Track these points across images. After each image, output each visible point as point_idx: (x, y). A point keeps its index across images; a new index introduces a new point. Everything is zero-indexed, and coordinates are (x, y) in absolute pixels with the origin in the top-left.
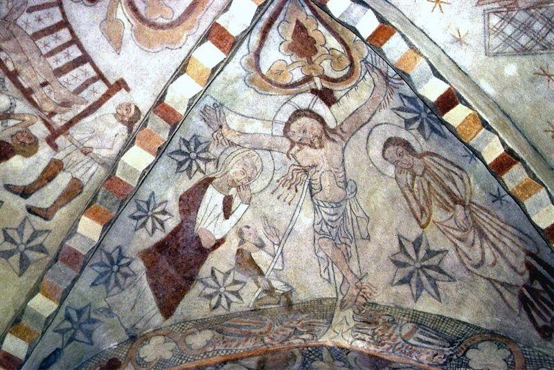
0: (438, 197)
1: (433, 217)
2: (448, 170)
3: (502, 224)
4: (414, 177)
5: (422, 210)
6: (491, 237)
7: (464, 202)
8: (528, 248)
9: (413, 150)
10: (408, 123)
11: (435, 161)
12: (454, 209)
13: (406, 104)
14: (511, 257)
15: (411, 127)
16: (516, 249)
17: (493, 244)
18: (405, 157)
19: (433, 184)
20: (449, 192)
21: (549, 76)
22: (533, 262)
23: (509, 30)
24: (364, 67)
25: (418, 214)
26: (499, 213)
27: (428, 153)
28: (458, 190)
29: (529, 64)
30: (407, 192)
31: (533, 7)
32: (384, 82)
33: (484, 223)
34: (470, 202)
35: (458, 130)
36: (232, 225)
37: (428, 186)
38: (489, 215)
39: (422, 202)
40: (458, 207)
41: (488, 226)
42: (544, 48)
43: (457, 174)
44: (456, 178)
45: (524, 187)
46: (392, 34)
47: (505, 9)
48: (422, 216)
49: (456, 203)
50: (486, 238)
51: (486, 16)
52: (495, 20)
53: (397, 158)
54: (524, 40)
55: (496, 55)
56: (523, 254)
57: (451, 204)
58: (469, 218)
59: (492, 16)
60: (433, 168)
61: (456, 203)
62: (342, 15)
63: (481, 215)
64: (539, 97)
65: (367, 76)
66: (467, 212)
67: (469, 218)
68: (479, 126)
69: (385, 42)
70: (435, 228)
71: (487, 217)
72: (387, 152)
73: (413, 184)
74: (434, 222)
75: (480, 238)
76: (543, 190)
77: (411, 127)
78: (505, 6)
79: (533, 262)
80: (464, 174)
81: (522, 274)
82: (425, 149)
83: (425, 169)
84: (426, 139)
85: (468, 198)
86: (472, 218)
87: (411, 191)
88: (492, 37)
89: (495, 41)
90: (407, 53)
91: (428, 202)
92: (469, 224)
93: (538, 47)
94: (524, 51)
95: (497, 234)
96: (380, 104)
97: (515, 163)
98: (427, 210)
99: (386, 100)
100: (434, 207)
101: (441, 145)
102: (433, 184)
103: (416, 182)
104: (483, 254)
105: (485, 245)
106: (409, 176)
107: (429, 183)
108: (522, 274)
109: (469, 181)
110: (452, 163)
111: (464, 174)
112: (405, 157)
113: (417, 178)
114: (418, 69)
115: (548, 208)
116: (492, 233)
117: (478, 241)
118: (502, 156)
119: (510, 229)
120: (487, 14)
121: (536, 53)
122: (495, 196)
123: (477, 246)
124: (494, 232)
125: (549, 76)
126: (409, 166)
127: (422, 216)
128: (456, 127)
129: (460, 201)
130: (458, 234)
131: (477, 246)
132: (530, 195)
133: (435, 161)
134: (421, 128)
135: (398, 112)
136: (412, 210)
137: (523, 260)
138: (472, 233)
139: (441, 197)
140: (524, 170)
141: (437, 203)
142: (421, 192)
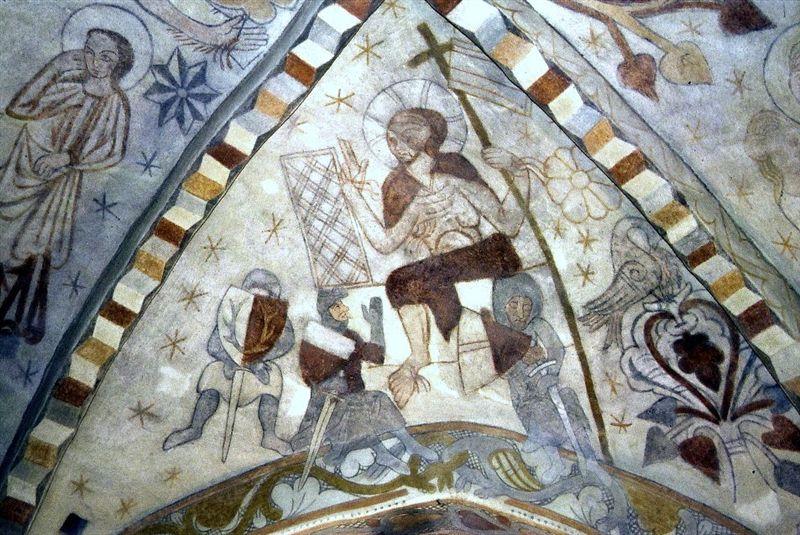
0: (65, 125)
1: (31, 124)
2: (113, 134)
3: (69, 216)
4: (79, 81)
5: (33, 104)
6: (43, 208)
7: (78, 163)
8: (54, 255)
9: (121, 75)
10: (163, 69)
11: (118, 112)
12: (60, 151)
13: (192, 70)
14: (29, 235)
15: (157, 74)
16: (44, 241)
17: (34, 212)
18: (105, 65)
19: (82, 113)
20: (82, 139)
21: (274, 231)
22: (39, 266)
23: (316, 178)
24: (234, 14)
25: (23, 100)
26: (82, 210)
27: (124, 99)
28: (90, 152)
29: (282, 207)
30: (49, 73)
31: (346, 199)
32: (219, 43)
33: (59, 194)
34: (81, 172)
35: (197, 175)
36: (256, 432)
37: (76, 106)
38: (73, 197)
39: (45, 101)
40: (65, 158)
41: (57, 200)
42: (305, 220)
43: (113, 147)
44: (107, 147)
45: (151, 264)
46: (304, 82)
47: (339, 171)
48: (24, 105)
49: (70, 152)
50: (39, 202)
51: (327, 151)
52: (325, 161)
53: (97, 51)
54: (308, 195)
55: (284, 167)
56: (42, 250)
57: (66, 147)
58: (56, 174)
59: (329, 157)
60: (106, 109)
61: (70, 152)
62: (321, 21)
63: (66, 194)
64: (247, 224)
65: (222, 18)
66: (65, 170)
67: (56, 174)
68: (209, 197)
69: (292, 76)
70: (17, 130)
71: (70, 195)
72: (104, 36)
73: (65, 80)
74: (25, 126)
75: (35, 195)
76: (157, 283)
77: (157, 74)
78: (342, 170)
79: (39, 266)
80: (117, 158)
81: (13, 256)
82: (130, 95)
83: (100, 98)
84: (146, 95)
85: (87, 167)
86: (60, 177)
87: (54, 79)
88: (304, 160)
89: (300, 165)
90: (281, 103)
91: (52, 108)
92: (49, 176)
93: (304, 213)
94: (296, 198)
95: (51, 214)
96: (182, 32)
97: (176, 244)
98: (36, 112)
99: (189, 42)
100: (55, 121)
101: (147, 122)
102: (82, 113)
103: (73, 84)
104: (14, 203)
105: (28, 204)
106: (77, 73)
107: (80, 106)
108: (13, 256)
109: (111, 166)
110: (126, 139)
111: (117, 158)
112: (105, 65)
113: (79, 85)
114: (263, 118)
115: (139, 295)
116: (50, 207)
117: (29, 192)
118: (178, 229)
119: (68, 227)
120: (330, 150)
121: (296, 212)
122: (104, 202)
123: (21, 194)
124: (53, 209)
125: (274, 231)
126: (92, 72)
127: (24, 105)
128: (200, 171)
129: (76, 158)
130: (25, 162)
131: (21, 194)
132: (145, 272)
133: (118, 112)
134: (159, 88)
135: (175, 58)
136: (25, 88)
137: (34, 252)
138: (37, 182)
139: (69, 129)
140: (171, 255)
141: (56, 125)
142: (60, 97)
